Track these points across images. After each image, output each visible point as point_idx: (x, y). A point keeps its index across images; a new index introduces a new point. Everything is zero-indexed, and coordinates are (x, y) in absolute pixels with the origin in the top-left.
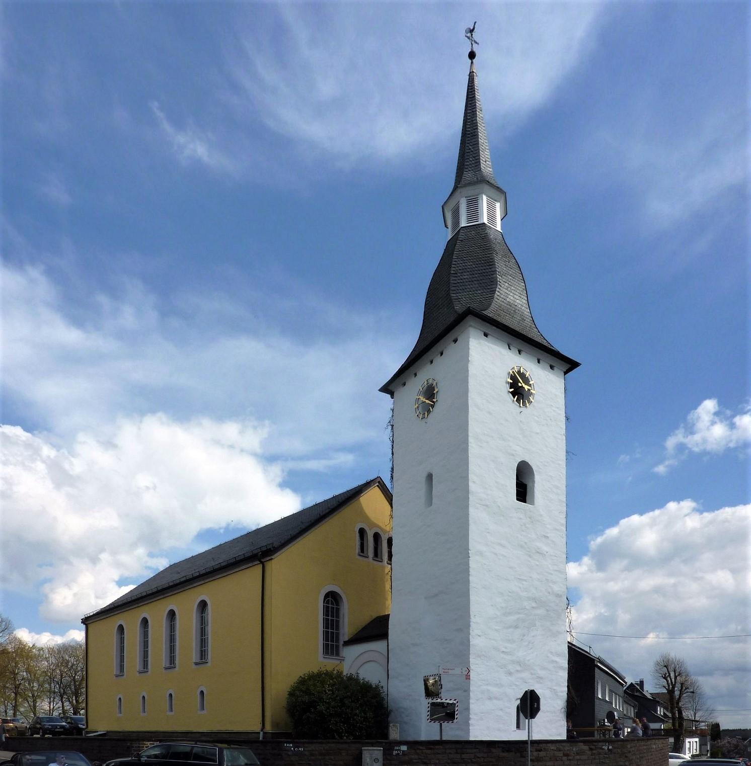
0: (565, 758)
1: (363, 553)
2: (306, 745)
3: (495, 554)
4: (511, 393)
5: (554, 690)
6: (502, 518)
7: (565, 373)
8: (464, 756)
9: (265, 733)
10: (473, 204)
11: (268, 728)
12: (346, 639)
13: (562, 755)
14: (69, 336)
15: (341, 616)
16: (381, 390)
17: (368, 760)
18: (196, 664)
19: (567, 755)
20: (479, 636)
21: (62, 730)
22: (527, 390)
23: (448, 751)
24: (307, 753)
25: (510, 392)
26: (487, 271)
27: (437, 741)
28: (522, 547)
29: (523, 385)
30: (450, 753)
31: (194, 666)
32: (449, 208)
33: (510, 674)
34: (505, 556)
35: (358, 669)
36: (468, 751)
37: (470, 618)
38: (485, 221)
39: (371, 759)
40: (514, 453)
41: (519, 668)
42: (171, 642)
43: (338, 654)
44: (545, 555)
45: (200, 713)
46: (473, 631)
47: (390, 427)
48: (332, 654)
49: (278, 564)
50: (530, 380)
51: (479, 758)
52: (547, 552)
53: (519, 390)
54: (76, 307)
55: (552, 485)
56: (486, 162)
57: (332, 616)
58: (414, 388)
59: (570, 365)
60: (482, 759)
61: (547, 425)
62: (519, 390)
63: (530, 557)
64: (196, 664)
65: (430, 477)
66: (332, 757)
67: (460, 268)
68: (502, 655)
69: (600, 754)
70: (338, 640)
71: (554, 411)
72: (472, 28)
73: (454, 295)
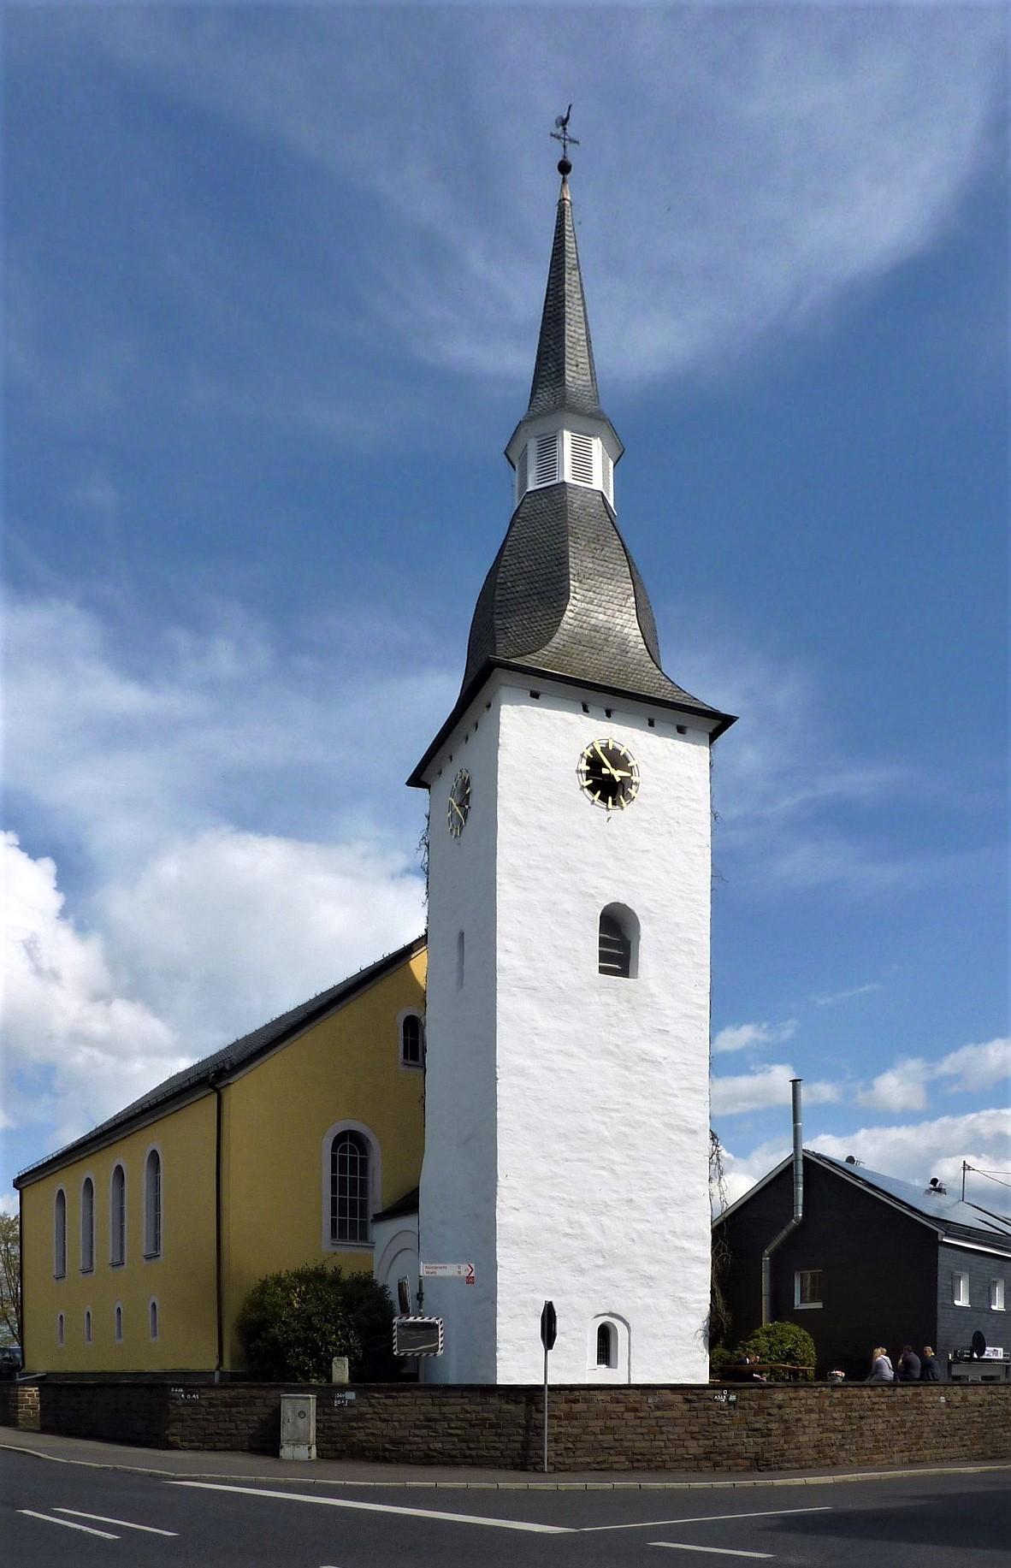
3: (552, 1070)
6: (567, 1007)
7: (713, 736)
8: (446, 1409)
10: (549, 446)
11: (227, 1366)
14: (125, 697)
15: (370, 1172)
18: (148, 1258)
19: (635, 1410)
24: (204, 1403)
28: (611, 1053)
29: (613, 771)
32: (513, 458)
33: (582, 1271)
36: (451, 1401)
38: (568, 477)
41: (600, 1262)
43: (364, 1237)
48: (353, 1237)
49: (242, 1091)
53: (606, 781)
54: (134, 649)
58: (446, 783)
62: (606, 781)
64: (148, 1258)
68: (564, 1240)
69: (708, 1409)
70: (364, 1213)
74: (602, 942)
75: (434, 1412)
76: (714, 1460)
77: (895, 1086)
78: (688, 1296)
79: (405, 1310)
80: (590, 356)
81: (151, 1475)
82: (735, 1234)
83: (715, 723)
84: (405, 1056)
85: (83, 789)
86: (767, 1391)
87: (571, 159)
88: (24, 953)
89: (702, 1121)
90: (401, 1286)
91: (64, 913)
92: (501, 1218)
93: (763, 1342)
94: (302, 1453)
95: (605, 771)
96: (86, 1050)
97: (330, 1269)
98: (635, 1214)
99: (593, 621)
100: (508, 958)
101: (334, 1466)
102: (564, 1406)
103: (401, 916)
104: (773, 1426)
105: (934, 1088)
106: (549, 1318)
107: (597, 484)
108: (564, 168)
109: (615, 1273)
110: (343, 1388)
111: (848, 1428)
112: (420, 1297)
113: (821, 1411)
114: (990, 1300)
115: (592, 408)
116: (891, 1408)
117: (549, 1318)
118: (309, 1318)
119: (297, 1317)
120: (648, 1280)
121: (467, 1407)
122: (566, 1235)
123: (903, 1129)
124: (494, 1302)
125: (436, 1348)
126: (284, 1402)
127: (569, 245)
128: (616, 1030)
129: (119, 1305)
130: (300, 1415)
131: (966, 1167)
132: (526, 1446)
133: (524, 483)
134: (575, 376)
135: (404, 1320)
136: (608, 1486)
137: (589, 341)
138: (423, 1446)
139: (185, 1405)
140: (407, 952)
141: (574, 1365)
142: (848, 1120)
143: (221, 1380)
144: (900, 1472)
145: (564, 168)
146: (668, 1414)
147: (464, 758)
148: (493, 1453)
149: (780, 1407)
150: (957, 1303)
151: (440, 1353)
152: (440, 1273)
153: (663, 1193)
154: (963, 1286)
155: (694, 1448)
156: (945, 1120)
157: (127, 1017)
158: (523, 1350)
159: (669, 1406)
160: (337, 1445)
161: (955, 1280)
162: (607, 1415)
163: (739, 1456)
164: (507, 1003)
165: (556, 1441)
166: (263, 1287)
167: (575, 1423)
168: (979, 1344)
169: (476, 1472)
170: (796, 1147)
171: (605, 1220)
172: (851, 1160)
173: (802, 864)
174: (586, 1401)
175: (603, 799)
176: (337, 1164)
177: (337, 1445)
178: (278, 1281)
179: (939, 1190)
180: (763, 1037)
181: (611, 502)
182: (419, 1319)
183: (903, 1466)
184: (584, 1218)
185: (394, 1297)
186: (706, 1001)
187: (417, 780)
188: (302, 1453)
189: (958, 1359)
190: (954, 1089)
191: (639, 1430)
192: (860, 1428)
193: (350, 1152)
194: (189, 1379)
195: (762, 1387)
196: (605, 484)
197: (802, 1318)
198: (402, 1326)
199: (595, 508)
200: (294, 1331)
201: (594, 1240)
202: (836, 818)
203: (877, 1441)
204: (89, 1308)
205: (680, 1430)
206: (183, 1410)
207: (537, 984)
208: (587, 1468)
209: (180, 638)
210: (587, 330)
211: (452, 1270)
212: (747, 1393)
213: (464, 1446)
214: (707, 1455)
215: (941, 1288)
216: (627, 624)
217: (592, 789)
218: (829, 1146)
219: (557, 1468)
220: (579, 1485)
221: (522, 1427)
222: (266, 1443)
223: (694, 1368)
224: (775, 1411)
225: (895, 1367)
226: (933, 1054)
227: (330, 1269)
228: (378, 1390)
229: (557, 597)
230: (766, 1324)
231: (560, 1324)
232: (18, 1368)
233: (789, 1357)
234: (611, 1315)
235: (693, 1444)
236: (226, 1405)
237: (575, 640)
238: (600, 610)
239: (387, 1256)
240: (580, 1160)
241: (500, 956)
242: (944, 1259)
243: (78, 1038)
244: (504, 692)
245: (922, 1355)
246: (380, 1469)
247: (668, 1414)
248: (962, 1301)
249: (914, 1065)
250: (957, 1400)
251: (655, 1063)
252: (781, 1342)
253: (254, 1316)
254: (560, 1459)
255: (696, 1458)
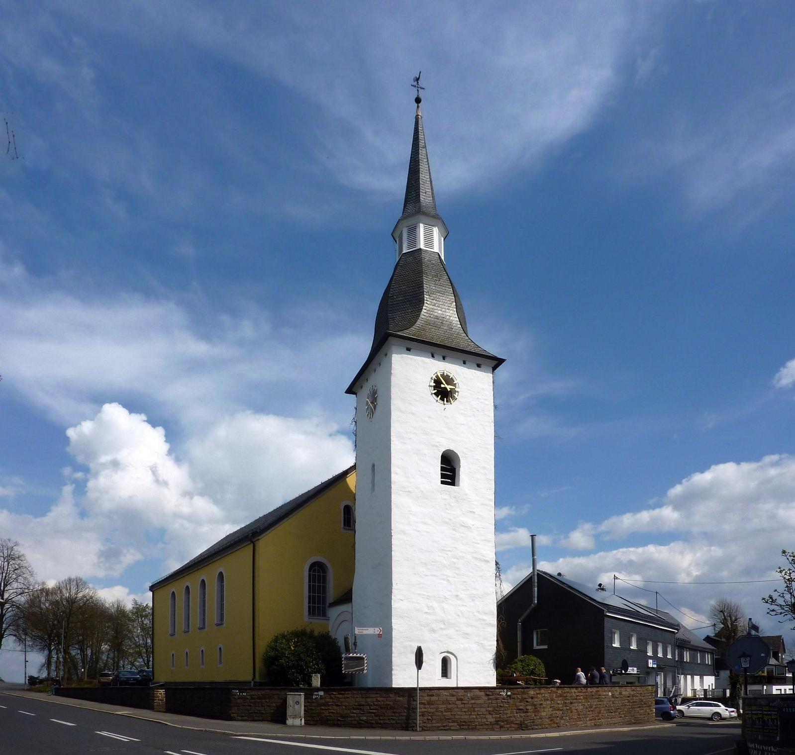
0: (459, 702)
1: (350, 527)
2: (248, 691)
4: (435, 394)
5: (482, 644)
7: (494, 368)
8: (369, 700)
9: (254, 682)
10: (413, 231)
11: (257, 679)
12: (332, 601)
13: (456, 699)
14: (199, 348)
16: (346, 392)
17: (291, 702)
19: (461, 700)
20: (402, 600)
21: (135, 682)
22: (449, 390)
23: (355, 696)
24: (248, 697)
25: (434, 393)
26: (417, 292)
27: (775, 685)
28: (446, 523)
30: (357, 697)
31: (216, 627)
32: (396, 236)
33: (434, 631)
34: (428, 532)
35: (25, 659)
37: (392, 586)
38: (422, 246)
39: (293, 701)
40: (437, 444)
41: (443, 626)
42: (222, 602)
43: (324, 615)
44: (471, 528)
45: (201, 667)
46: (395, 596)
47: (354, 423)
48: (319, 615)
49: (266, 543)
50: (455, 380)
51: (379, 701)
52: (473, 525)
53: (443, 391)
54: (204, 326)
55: (479, 467)
56: (426, 193)
57: (319, 582)
59: (495, 363)
60: (382, 702)
61: (474, 415)
62: (443, 391)
63: (455, 531)
65: (373, 466)
66: (267, 700)
67: (396, 291)
70: (324, 603)
71: (482, 403)
72: (418, 77)
73: (391, 315)
74: (442, 469)
75: (363, 701)
76: (500, 725)
77: (579, 538)
78: (485, 643)
79: (348, 650)
80: (432, 189)
81: (224, 733)
82: (510, 610)
83: (496, 362)
84: (344, 525)
85: (179, 393)
86: (526, 690)
87: (421, 96)
88: (150, 473)
89: (492, 557)
90: (346, 639)
91: (170, 452)
92: (395, 605)
93: (519, 665)
94: (297, 722)
95: (442, 386)
96: (180, 521)
97: (308, 630)
98: (460, 602)
99: (436, 314)
100: (397, 477)
101: (314, 729)
102: (427, 698)
103: (341, 457)
104: (529, 707)
105: (597, 537)
106: (419, 654)
107: (436, 250)
108: (418, 100)
109: (451, 632)
110: (317, 690)
111: (565, 708)
112: (355, 644)
113: (552, 700)
114: (630, 644)
115: (433, 213)
116: (586, 698)
117: (419, 654)
118: (299, 654)
119: (293, 654)
120: (466, 635)
121: (378, 699)
122: (426, 613)
123: (581, 558)
124: (391, 646)
125: (363, 670)
126: (289, 697)
127: (421, 137)
128: (449, 512)
129: (202, 648)
130: (296, 703)
131: (615, 578)
132: (408, 718)
133: (401, 249)
134: (425, 198)
135: (347, 655)
136: (450, 738)
137: (431, 181)
138: (357, 719)
139: (239, 698)
140: (345, 474)
141: (430, 677)
142: (554, 554)
143: (255, 685)
144: (591, 731)
145: (418, 100)
146: (477, 702)
147: (374, 380)
148: (392, 722)
149: (532, 698)
150: (614, 645)
151: (365, 672)
152: (365, 632)
153: (474, 592)
154: (617, 637)
155: (490, 719)
156: (602, 553)
157: (202, 505)
158: (405, 670)
159: (478, 698)
160: (314, 718)
161: (613, 634)
162: (447, 702)
163: (512, 722)
164: (397, 499)
165: (423, 716)
166: (276, 640)
167: (432, 706)
168: (625, 666)
169: (384, 732)
170: (534, 568)
171: (445, 606)
172: (559, 574)
173: (532, 427)
174: (438, 695)
175: (442, 399)
176: (311, 578)
177: (314, 718)
178: (283, 636)
179: (603, 589)
180: (513, 513)
181: (443, 258)
182: (355, 655)
183: (591, 727)
184: (435, 605)
185: (341, 643)
186: (493, 497)
187: (350, 391)
188: (297, 722)
189: (615, 674)
190: (607, 538)
191: (463, 710)
192: (570, 708)
193: (318, 571)
194: (242, 685)
195: (523, 688)
196: (440, 250)
197: (537, 653)
198: (346, 658)
199: (435, 261)
200: (292, 661)
201: (439, 614)
202: (545, 405)
203: (579, 715)
204: (187, 650)
205: (483, 710)
206: (239, 701)
207: (410, 490)
208: (438, 729)
209: (225, 319)
210: (430, 176)
211: (370, 631)
212: (516, 691)
213: (377, 718)
214: (497, 722)
215: (606, 638)
216: (452, 315)
217: (437, 394)
218: (546, 567)
219: (423, 729)
220: (435, 738)
221: (404, 709)
222: (279, 717)
223: (488, 678)
224: (529, 700)
225: (587, 678)
226: (597, 519)
227: (308, 630)
228: (335, 690)
229: (418, 302)
230: (520, 657)
231: (425, 658)
232: (150, 680)
233: (532, 673)
234: (448, 652)
235: (490, 716)
236: (259, 698)
237: (428, 323)
238: (439, 308)
239: (335, 624)
240: (432, 576)
241: (393, 475)
242: (607, 623)
243: (177, 515)
244: (394, 348)
245: (600, 671)
246: (336, 730)
247: (477, 702)
248: (616, 645)
249: (587, 526)
250: (617, 694)
251: (468, 527)
252: (528, 665)
253: (272, 654)
254: (425, 725)
255: (491, 724)
